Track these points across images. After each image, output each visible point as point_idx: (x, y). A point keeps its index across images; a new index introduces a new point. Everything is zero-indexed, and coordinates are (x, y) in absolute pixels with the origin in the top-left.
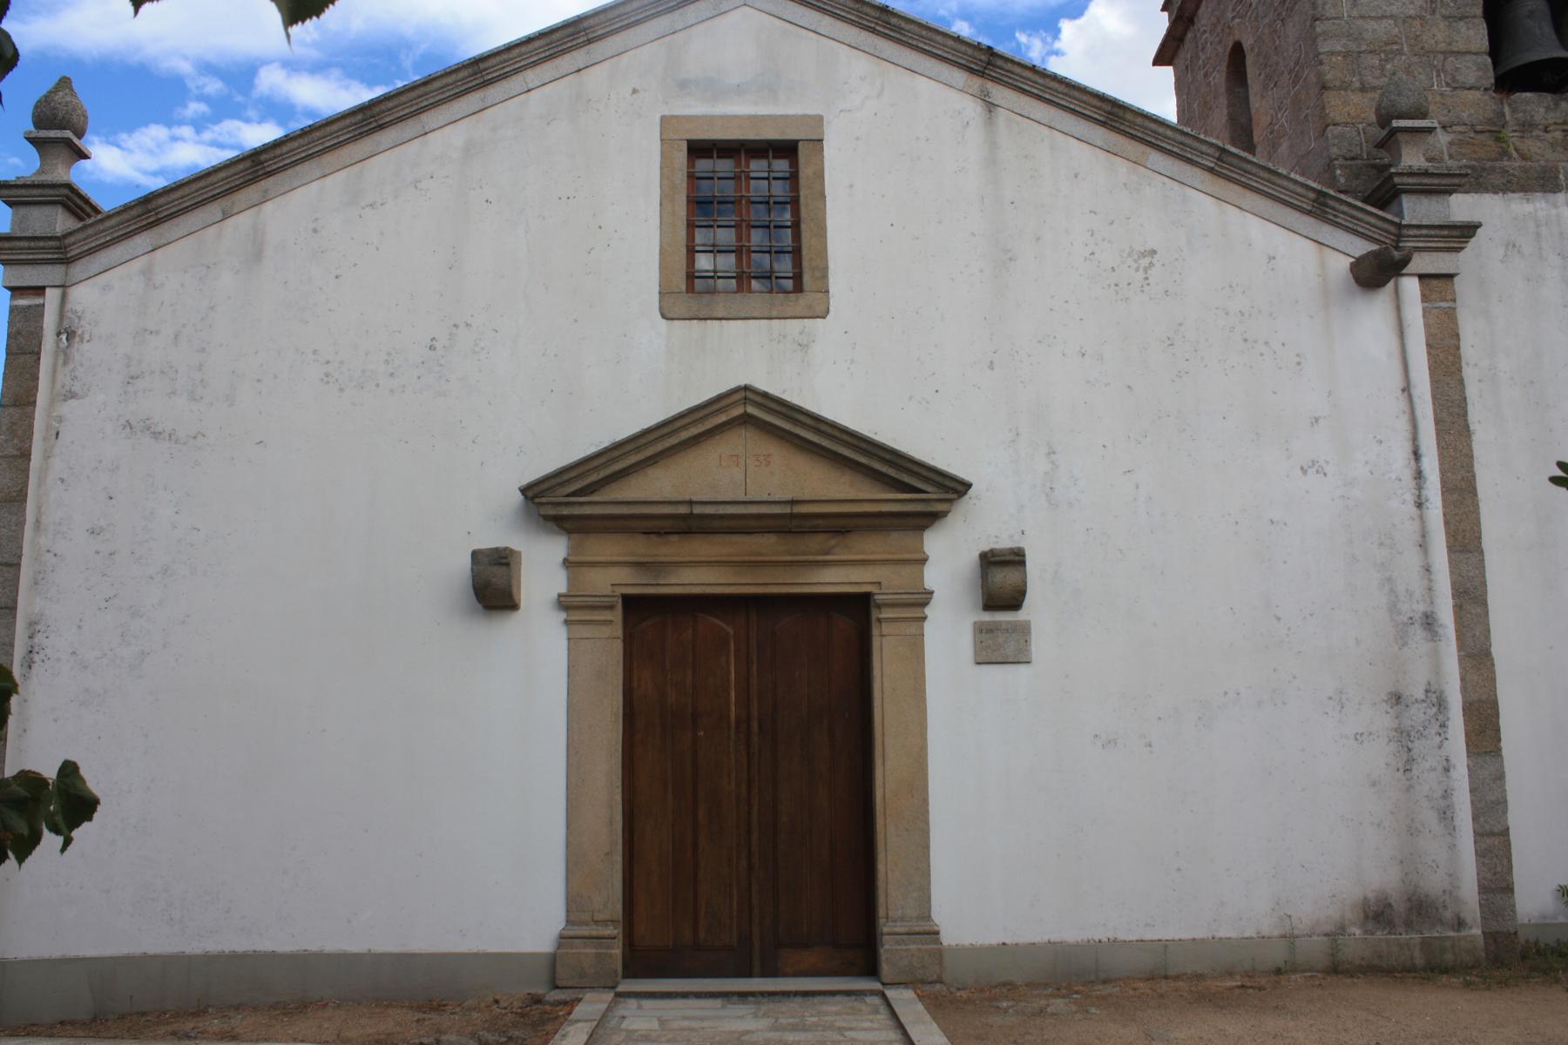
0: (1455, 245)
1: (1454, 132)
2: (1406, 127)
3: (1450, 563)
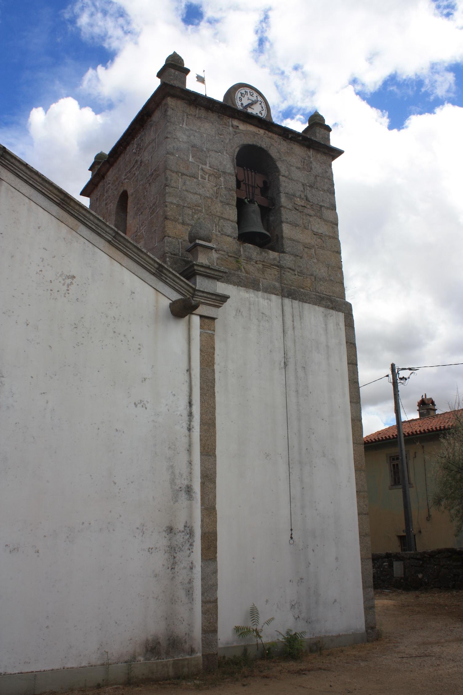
0: (217, 304)
1: (220, 254)
2: (201, 244)
3: (201, 460)
